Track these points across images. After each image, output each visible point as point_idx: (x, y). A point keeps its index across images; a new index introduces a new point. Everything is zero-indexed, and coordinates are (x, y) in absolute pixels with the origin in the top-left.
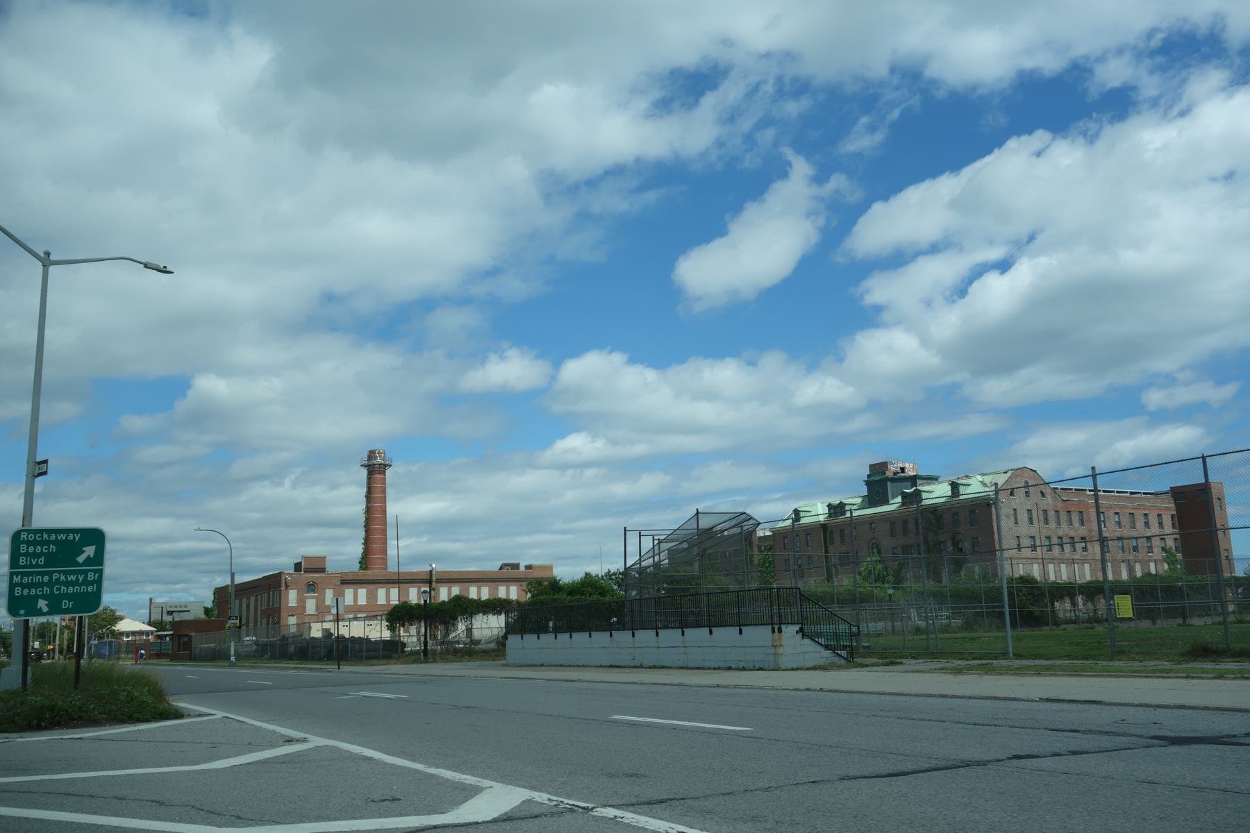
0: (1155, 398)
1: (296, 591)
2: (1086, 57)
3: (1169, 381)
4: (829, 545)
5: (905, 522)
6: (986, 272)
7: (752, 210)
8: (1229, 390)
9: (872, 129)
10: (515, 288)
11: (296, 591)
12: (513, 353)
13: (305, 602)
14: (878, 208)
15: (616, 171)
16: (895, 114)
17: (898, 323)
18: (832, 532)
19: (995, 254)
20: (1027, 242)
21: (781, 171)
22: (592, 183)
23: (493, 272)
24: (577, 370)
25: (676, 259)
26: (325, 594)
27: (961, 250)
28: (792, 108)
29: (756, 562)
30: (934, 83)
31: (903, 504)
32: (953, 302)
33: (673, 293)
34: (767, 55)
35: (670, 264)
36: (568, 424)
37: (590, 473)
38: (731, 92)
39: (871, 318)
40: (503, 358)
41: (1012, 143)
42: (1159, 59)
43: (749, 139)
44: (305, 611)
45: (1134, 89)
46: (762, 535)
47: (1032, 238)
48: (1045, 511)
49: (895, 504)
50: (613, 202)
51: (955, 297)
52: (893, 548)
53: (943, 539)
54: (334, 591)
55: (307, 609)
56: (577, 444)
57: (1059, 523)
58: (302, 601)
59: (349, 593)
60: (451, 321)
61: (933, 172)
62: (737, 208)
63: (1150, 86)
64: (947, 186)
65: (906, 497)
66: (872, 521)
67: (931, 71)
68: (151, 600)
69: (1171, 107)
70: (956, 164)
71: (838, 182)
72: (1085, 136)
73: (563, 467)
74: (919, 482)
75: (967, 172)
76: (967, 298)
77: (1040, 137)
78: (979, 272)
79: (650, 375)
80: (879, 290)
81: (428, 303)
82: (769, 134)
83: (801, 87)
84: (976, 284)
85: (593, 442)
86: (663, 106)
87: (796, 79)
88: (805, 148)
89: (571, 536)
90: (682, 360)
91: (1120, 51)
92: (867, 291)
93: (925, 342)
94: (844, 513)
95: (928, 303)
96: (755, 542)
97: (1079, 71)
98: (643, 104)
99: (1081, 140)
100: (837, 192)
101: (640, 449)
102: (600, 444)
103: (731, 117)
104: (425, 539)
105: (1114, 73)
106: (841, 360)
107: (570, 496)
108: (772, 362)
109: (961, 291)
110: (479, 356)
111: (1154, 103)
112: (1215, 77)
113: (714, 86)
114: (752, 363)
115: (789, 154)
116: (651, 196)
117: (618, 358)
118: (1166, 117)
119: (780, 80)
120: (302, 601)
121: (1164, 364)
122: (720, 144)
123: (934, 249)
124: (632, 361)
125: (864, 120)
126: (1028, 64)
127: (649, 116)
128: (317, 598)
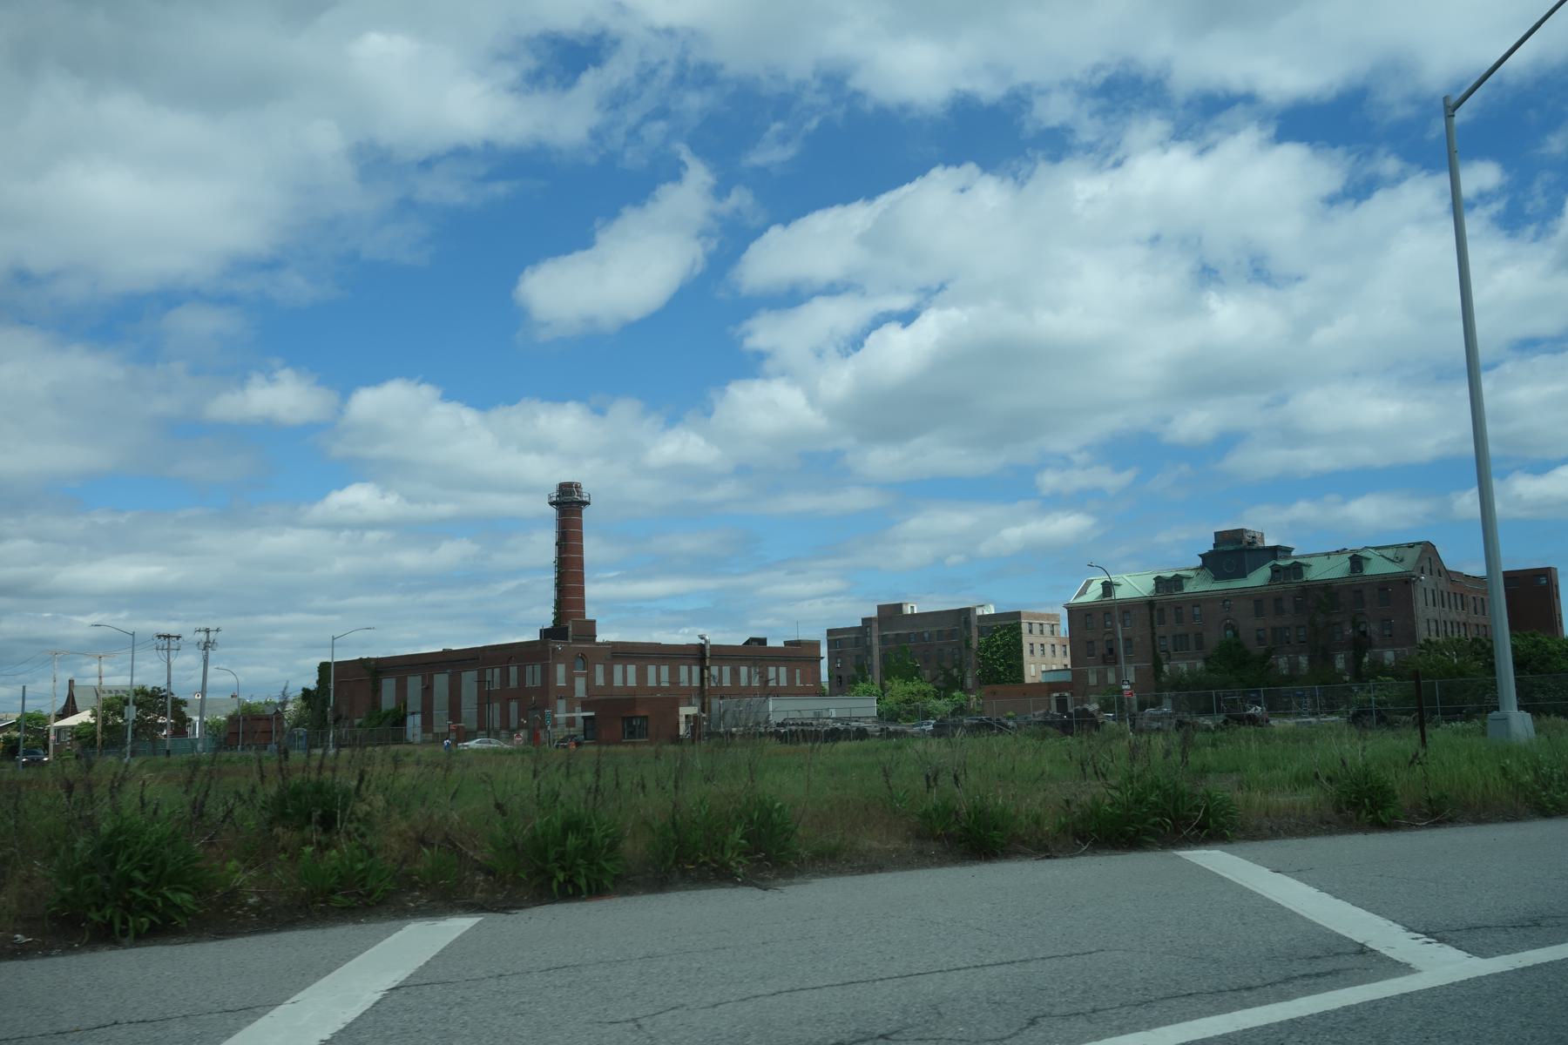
0: (1050, 480)
1: (564, 665)
2: (1028, 87)
3: (1064, 462)
4: (1156, 625)
5: (1278, 600)
6: (886, 322)
7: (631, 218)
8: (1127, 476)
9: (784, 139)
10: (296, 287)
11: (564, 665)
12: (286, 375)
13: (574, 681)
14: (775, 232)
15: (460, 153)
16: (814, 123)
17: (783, 373)
18: (1162, 610)
19: (901, 303)
20: (931, 294)
21: (675, 173)
22: (427, 164)
23: (271, 265)
24: (368, 402)
25: (521, 270)
26: (595, 670)
27: (864, 294)
28: (694, 102)
29: (975, 645)
30: (858, 94)
31: (1273, 579)
32: (848, 355)
33: (517, 316)
34: (669, 32)
35: (512, 280)
36: (350, 472)
37: (373, 536)
38: (617, 71)
39: (752, 366)
40: (271, 380)
41: (937, 173)
42: (1103, 101)
43: (634, 133)
44: (574, 694)
45: (1071, 131)
46: (981, 613)
47: (942, 288)
48: (1442, 592)
49: (1259, 578)
50: (446, 190)
51: (850, 350)
52: (1258, 630)
53: (1338, 620)
54: (605, 668)
55: (576, 691)
56: (359, 498)
57: (1450, 607)
58: (570, 679)
59: (618, 670)
60: (198, 323)
61: (847, 199)
62: (612, 214)
63: (1088, 131)
64: (858, 216)
65: (1277, 571)
66: (1225, 599)
67: (857, 82)
68: (71, 682)
69: (1107, 156)
70: (870, 192)
71: (740, 198)
72: (1016, 178)
73: (335, 526)
74: (1279, 554)
75: (884, 200)
76: (861, 352)
77: (971, 168)
78: (880, 321)
79: (469, 416)
80: (764, 333)
81: (170, 297)
82: (658, 128)
83: (706, 76)
84: (874, 336)
85: (383, 497)
86: (534, 80)
87: (703, 67)
88: (702, 149)
89: (336, 618)
90: (511, 401)
91: (1065, 85)
92: (749, 333)
93: (812, 399)
94: (1181, 587)
95: (819, 353)
96: (974, 622)
97: (1019, 100)
98: (511, 73)
99: (1010, 181)
100: (738, 211)
101: (445, 509)
102: (392, 500)
103: (616, 101)
104: (124, 615)
105: (1055, 110)
106: (709, 414)
107: (340, 565)
108: (624, 412)
109: (856, 343)
110: (237, 375)
111: (1090, 148)
112: (1156, 127)
113: (598, 62)
114: (600, 411)
115: (685, 154)
116: (500, 188)
117: (426, 391)
118: (1099, 168)
119: (682, 63)
120: (570, 679)
121: (1059, 444)
122: (596, 135)
123: (832, 290)
124: (447, 397)
125: (777, 126)
126: (965, 85)
127: (513, 89)
128: (587, 676)
